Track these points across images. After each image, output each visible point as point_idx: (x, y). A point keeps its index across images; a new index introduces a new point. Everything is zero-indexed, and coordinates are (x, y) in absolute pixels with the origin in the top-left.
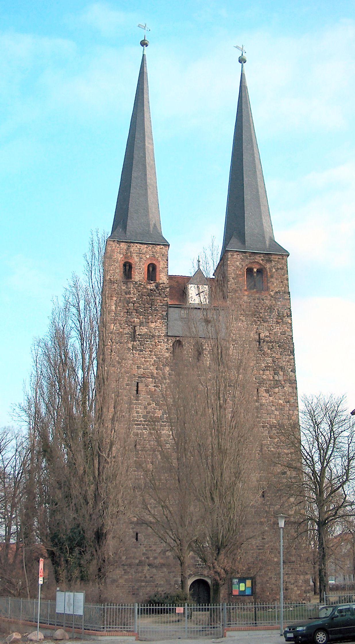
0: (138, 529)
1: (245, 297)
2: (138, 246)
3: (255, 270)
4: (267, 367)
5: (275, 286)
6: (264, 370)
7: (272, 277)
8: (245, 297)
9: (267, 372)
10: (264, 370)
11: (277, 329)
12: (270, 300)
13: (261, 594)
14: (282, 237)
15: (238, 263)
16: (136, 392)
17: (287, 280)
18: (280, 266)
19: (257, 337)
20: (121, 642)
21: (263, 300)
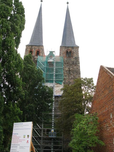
0: (24, 139)
1: (65, 59)
2: (35, 46)
3: (69, 51)
4: (72, 78)
5: (75, 55)
6: (71, 79)
7: (74, 53)
8: (65, 59)
9: (72, 80)
10: (71, 79)
11: (75, 67)
12: (73, 59)
13: (91, 112)
14: (77, 43)
15: (63, 50)
16: (28, 147)
17: (79, 54)
18: (76, 50)
19: (69, 70)
20: (1, 109)
21: (71, 59)
